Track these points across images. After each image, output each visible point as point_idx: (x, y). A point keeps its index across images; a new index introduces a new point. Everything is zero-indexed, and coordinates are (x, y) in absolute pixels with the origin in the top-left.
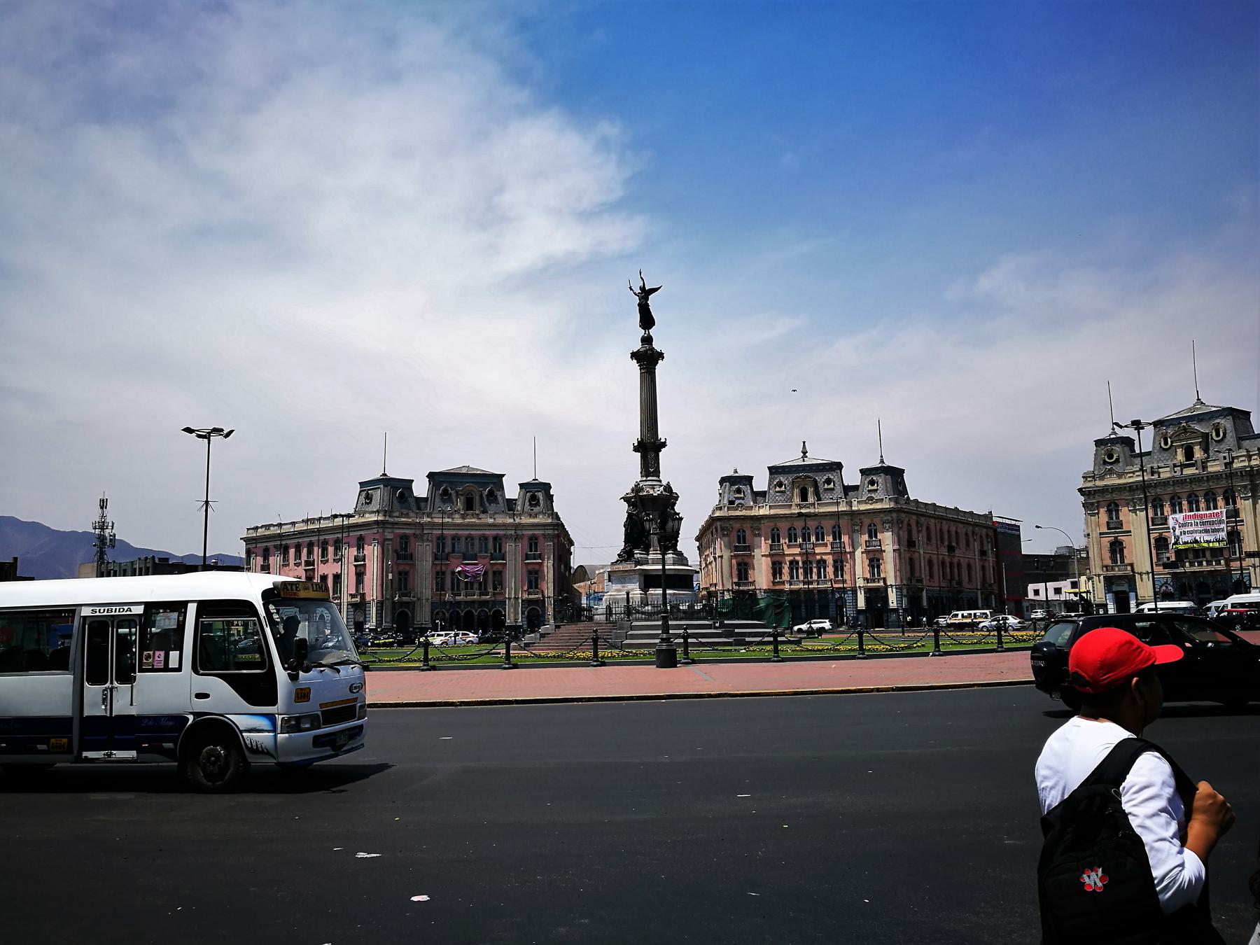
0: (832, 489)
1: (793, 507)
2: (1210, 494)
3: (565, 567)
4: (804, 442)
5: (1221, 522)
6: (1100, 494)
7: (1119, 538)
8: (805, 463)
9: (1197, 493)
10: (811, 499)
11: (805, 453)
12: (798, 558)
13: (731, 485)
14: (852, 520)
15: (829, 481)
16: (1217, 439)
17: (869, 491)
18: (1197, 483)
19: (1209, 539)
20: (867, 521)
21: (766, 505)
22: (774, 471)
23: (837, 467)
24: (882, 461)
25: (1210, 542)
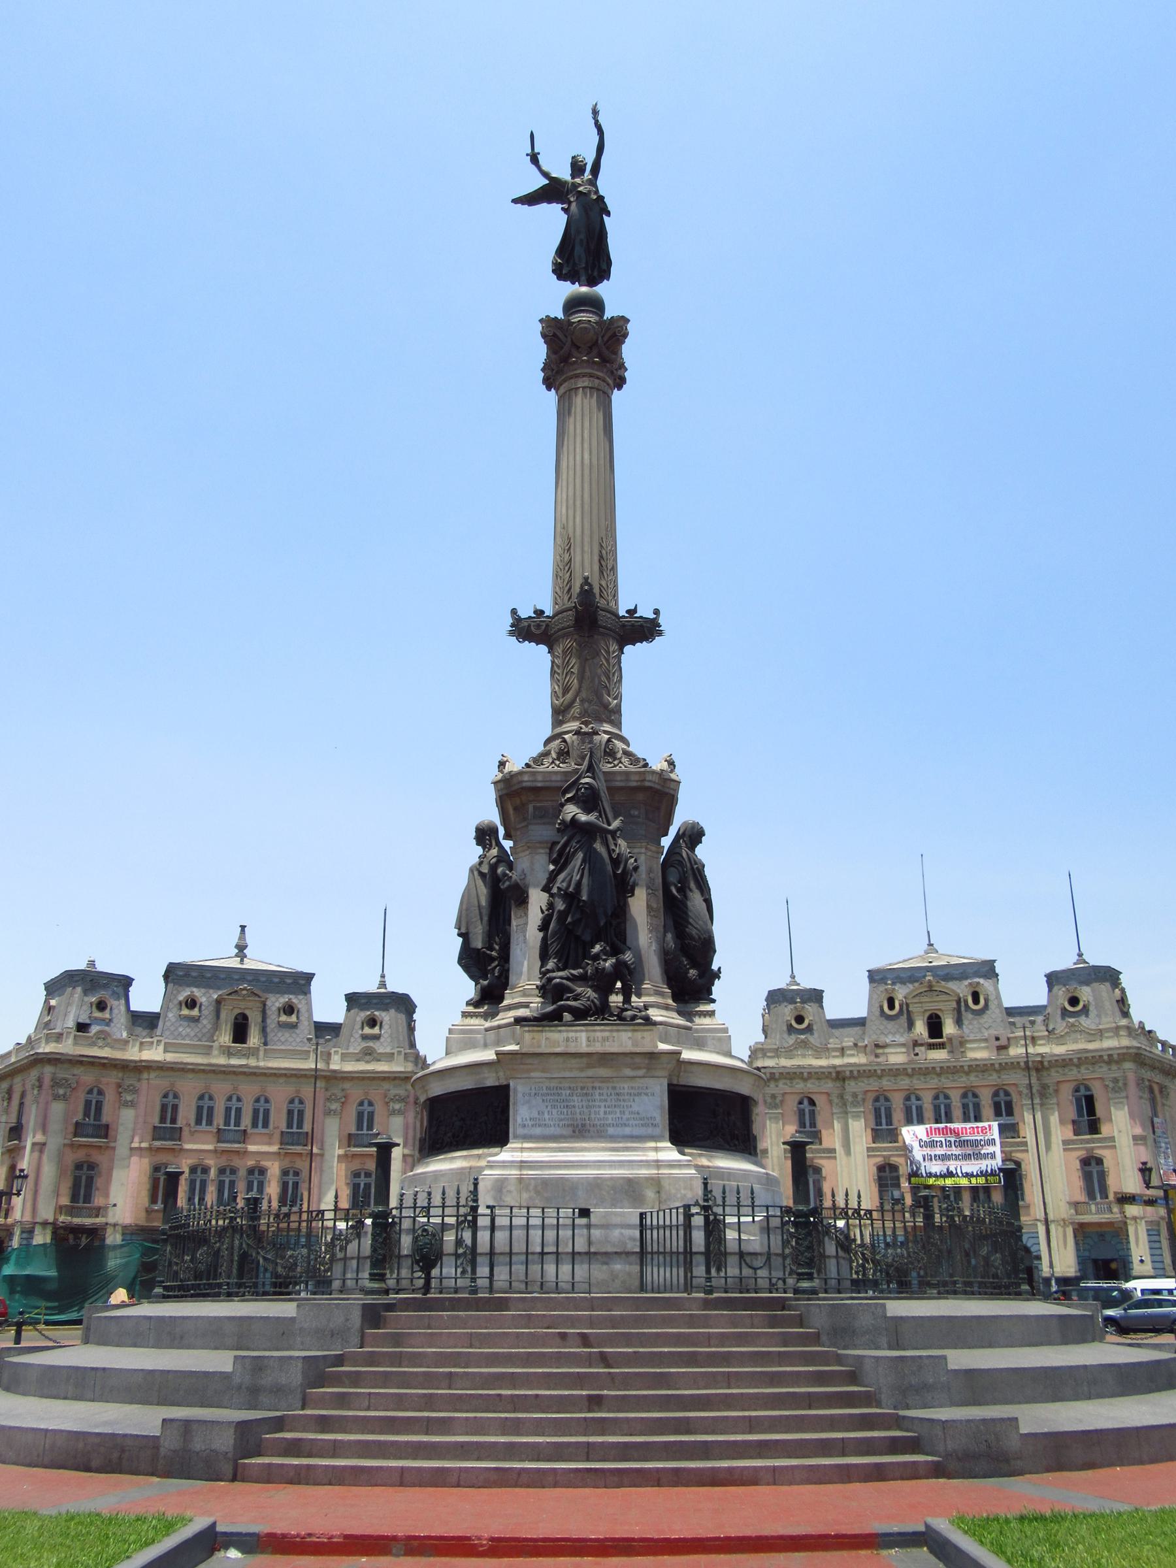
0: (294, 1026)
1: (215, 1052)
2: (970, 1095)
3: (388, 1004)
4: (243, 927)
5: (992, 1142)
6: (788, 1082)
7: (892, 1159)
8: (244, 967)
9: (921, 1093)
10: (254, 1039)
11: (241, 948)
12: (210, 1162)
13: (86, 992)
14: (327, 1090)
15: (289, 1009)
16: (893, 1013)
17: (365, 1037)
18: (950, 1076)
19: (969, 1171)
20: (356, 1093)
21: (159, 1042)
22: (175, 974)
23: (301, 982)
24: (383, 984)
25: (972, 1175)
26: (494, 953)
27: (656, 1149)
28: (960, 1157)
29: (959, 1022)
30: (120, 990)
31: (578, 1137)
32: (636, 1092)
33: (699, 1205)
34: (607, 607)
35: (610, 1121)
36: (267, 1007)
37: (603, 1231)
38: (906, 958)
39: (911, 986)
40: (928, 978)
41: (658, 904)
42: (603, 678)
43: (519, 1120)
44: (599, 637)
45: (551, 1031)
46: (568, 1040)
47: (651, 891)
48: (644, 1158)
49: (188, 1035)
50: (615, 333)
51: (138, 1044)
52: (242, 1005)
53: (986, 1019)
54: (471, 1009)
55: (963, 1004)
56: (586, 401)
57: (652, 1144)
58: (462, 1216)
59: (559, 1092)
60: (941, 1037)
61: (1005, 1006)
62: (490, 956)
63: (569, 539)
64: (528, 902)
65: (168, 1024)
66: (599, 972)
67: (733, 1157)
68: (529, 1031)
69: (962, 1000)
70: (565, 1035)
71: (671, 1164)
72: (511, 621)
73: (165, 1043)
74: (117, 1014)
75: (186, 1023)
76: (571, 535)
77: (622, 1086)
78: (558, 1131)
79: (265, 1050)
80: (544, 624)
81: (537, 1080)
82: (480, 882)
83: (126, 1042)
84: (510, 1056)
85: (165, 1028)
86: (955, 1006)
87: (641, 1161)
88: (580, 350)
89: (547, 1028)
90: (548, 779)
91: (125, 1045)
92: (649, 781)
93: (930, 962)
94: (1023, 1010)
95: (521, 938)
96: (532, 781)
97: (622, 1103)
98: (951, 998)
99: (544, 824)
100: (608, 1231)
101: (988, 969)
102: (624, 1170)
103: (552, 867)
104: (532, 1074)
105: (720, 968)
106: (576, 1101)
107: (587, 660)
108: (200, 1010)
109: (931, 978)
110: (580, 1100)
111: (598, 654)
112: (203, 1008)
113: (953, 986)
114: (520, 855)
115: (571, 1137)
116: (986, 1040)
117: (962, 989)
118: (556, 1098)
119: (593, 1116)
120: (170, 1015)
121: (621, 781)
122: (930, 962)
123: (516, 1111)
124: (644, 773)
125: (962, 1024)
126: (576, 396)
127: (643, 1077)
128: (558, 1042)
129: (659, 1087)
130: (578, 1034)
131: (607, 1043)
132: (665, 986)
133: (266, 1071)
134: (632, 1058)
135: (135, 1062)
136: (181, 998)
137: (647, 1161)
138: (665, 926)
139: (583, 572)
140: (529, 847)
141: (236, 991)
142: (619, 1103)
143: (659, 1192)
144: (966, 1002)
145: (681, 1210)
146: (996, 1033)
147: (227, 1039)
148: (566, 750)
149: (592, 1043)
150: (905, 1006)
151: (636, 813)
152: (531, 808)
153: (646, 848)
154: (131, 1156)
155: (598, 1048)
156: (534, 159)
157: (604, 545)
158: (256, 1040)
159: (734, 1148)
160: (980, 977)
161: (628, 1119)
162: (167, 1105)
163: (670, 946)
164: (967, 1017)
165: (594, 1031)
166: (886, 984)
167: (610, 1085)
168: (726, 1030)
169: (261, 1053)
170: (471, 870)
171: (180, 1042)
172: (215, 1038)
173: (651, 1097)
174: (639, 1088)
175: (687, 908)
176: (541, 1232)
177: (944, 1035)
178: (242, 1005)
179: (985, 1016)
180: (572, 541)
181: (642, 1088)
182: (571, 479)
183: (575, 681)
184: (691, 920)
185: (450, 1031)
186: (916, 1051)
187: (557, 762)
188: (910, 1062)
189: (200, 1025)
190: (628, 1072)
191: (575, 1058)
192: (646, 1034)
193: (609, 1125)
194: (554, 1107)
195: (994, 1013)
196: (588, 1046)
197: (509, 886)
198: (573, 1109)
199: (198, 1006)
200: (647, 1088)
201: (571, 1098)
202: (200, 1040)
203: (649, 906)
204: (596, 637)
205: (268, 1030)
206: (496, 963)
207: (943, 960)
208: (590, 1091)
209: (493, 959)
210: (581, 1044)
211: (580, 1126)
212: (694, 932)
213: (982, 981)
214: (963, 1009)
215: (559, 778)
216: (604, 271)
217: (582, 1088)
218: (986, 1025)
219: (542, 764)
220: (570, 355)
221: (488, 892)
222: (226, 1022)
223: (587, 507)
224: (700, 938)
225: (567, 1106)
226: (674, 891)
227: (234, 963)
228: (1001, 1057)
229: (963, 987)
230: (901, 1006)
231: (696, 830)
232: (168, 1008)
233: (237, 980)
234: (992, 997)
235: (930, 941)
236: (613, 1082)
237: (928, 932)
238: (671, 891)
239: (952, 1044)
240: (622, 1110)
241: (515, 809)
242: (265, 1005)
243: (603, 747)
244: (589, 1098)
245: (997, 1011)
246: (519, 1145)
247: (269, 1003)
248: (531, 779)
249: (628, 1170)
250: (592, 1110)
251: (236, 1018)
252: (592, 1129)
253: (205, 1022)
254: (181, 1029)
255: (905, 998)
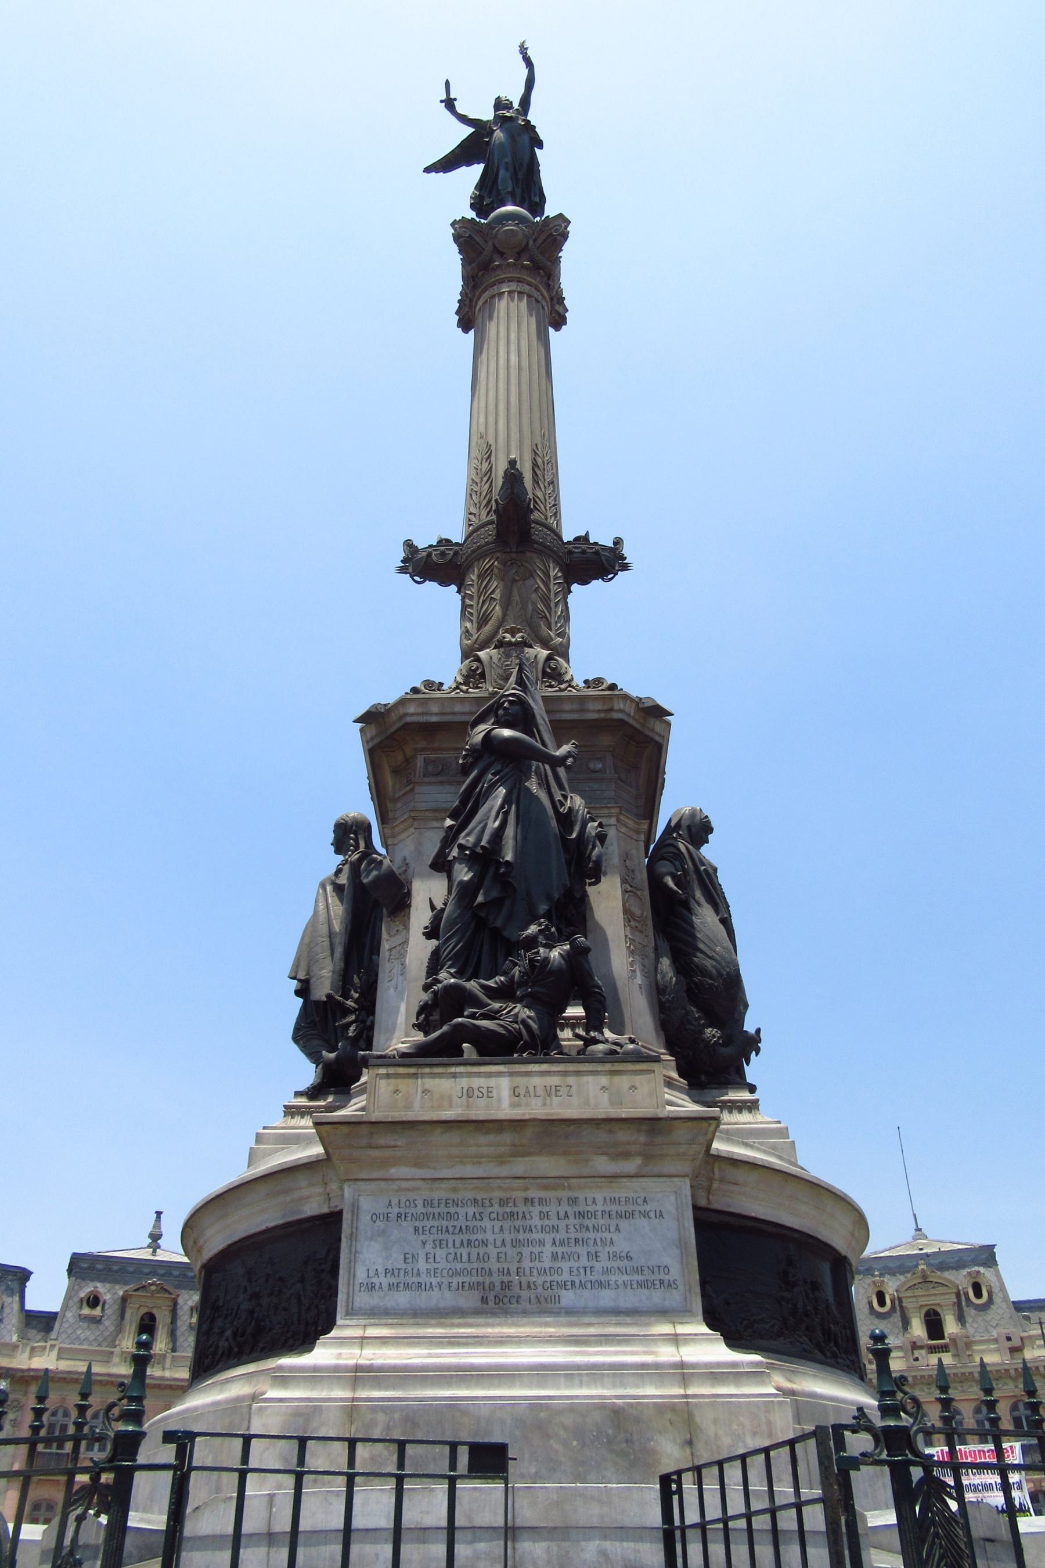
1: (116, 1359)
4: (159, 1214)
21: (53, 1346)
26: (350, 1003)
27: (676, 1340)
28: (980, 1488)
29: (961, 1319)
30: (15, 1285)
31: (493, 1314)
32: (622, 1209)
33: (870, 1429)
34: (544, 521)
35: (566, 1276)
36: (178, 1307)
37: (554, 1547)
38: (893, 1245)
39: (902, 1278)
40: (921, 1267)
41: (643, 909)
42: (541, 606)
43: (361, 1276)
44: (534, 555)
45: (434, 1076)
46: (470, 1093)
47: (629, 888)
48: (649, 1359)
49: (86, 1339)
50: (551, 233)
51: (28, 1349)
52: (150, 1303)
53: (992, 1314)
54: (303, 1101)
55: (963, 1298)
56: (513, 305)
57: (666, 1329)
58: (84, 1470)
59: (452, 1210)
60: (943, 1338)
61: (1011, 1300)
62: (341, 1006)
63: (489, 446)
64: (409, 906)
65: (65, 1325)
66: (539, 969)
67: (823, 1379)
68: (388, 1076)
69: (962, 1293)
70: (464, 1082)
71: (715, 1374)
72: (402, 555)
73: (60, 1349)
74: (9, 1314)
75: (85, 1325)
76: (491, 441)
77: (590, 1196)
78: (449, 1299)
79: (173, 1357)
80: (451, 553)
81: (404, 1184)
82: (333, 899)
83: (15, 1347)
84: (345, 1129)
85: (62, 1330)
86: (955, 1300)
87: (644, 1366)
88: (505, 256)
89: (427, 1070)
90: (448, 710)
91: (14, 1351)
92: (621, 711)
93: (921, 1249)
94: (1032, 1305)
95: (397, 968)
96: (423, 714)
97: (591, 1235)
98: (950, 1291)
99: (442, 783)
100: (565, 1544)
101: (986, 1255)
102: (603, 1386)
103: (449, 822)
104: (394, 1172)
105: (758, 1031)
106: (490, 1230)
107: (514, 581)
108: (103, 1310)
109: (924, 1267)
110: (497, 1230)
111: (532, 575)
112: (107, 1306)
113: (949, 1275)
114: (402, 837)
115: (477, 1312)
116: (996, 1341)
117: (961, 1279)
118: (445, 1223)
119: (526, 1264)
120: (69, 1314)
121: (572, 711)
122: (921, 1249)
123: (354, 1255)
124: (610, 698)
125: (965, 1322)
126: (499, 300)
127: (637, 1176)
128: (450, 1098)
129: (673, 1198)
130: (492, 1082)
131: (556, 1100)
132: (664, 1051)
133: (172, 1383)
134: (611, 1132)
135: (22, 1371)
136: (82, 1295)
137: (657, 1366)
138: (656, 949)
139: (508, 454)
140: (414, 819)
141: (144, 1287)
142: (585, 1235)
143: (690, 1443)
144: (966, 1294)
145: (808, 1452)
146: (1006, 1331)
147: (130, 1344)
148: (479, 671)
149: (524, 1100)
150: (897, 1303)
151: (599, 766)
152: (420, 761)
153: (618, 820)
154: (7, 1490)
155: (536, 1109)
156: (449, 104)
157: (540, 452)
158: (163, 1346)
159: (832, 1361)
160: (979, 1265)
161: (606, 1271)
162: (55, 1424)
163: (668, 978)
164: (970, 1313)
165: (528, 1074)
166: (873, 1276)
167: (564, 1194)
168: (784, 1133)
169: (168, 1361)
170: (323, 886)
171: (76, 1346)
172: (117, 1343)
173: (656, 1221)
174: (627, 1200)
175: (693, 927)
176: (388, 1549)
177: (946, 1335)
178: (150, 1303)
179: (991, 1312)
180: (493, 448)
181: (635, 1201)
182: (492, 384)
183: (497, 608)
184: (701, 946)
185: (259, 1138)
186: (916, 1355)
187: (464, 688)
188: (910, 1369)
189: (101, 1327)
190: (603, 1164)
191: (487, 1132)
192: (638, 1079)
193: (564, 1285)
194: (440, 1244)
195: (1000, 1308)
196: (513, 1105)
197: (377, 879)
198: (482, 1251)
199: (101, 1304)
200: (645, 1201)
201: (478, 1224)
202: (99, 1345)
203: (626, 911)
204: (528, 554)
205: (178, 1333)
206: (353, 1017)
207: (933, 1247)
208: (521, 1209)
209: (347, 1011)
210: (499, 1100)
211: (498, 1288)
212: (708, 963)
213: (982, 1270)
214: (964, 1303)
215: (467, 708)
216: (536, 204)
217: (503, 1202)
218: (994, 1323)
219: (439, 690)
220: (491, 261)
221: (346, 910)
222: (131, 1323)
223: (514, 410)
224: (720, 974)
225: (469, 1242)
226: (670, 881)
227: (146, 1255)
228: (1016, 1361)
229: (961, 1277)
230: (893, 1301)
231: (698, 818)
232: (67, 1306)
233: (147, 1274)
234: (996, 1290)
235: (917, 1226)
236: (570, 1188)
237: (915, 1215)
238: (666, 885)
239: (956, 1346)
240: (592, 1249)
241: (396, 771)
242: (175, 1304)
243: (540, 666)
244: (518, 1223)
245: (1004, 1306)
246: (358, 1332)
247: (180, 1301)
248: (420, 710)
249: (614, 1386)
250: (526, 1251)
251: (142, 1319)
252: (525, 1294)
253: (107, 1323)
254: (79, 1332)
255: (897, 1291)
